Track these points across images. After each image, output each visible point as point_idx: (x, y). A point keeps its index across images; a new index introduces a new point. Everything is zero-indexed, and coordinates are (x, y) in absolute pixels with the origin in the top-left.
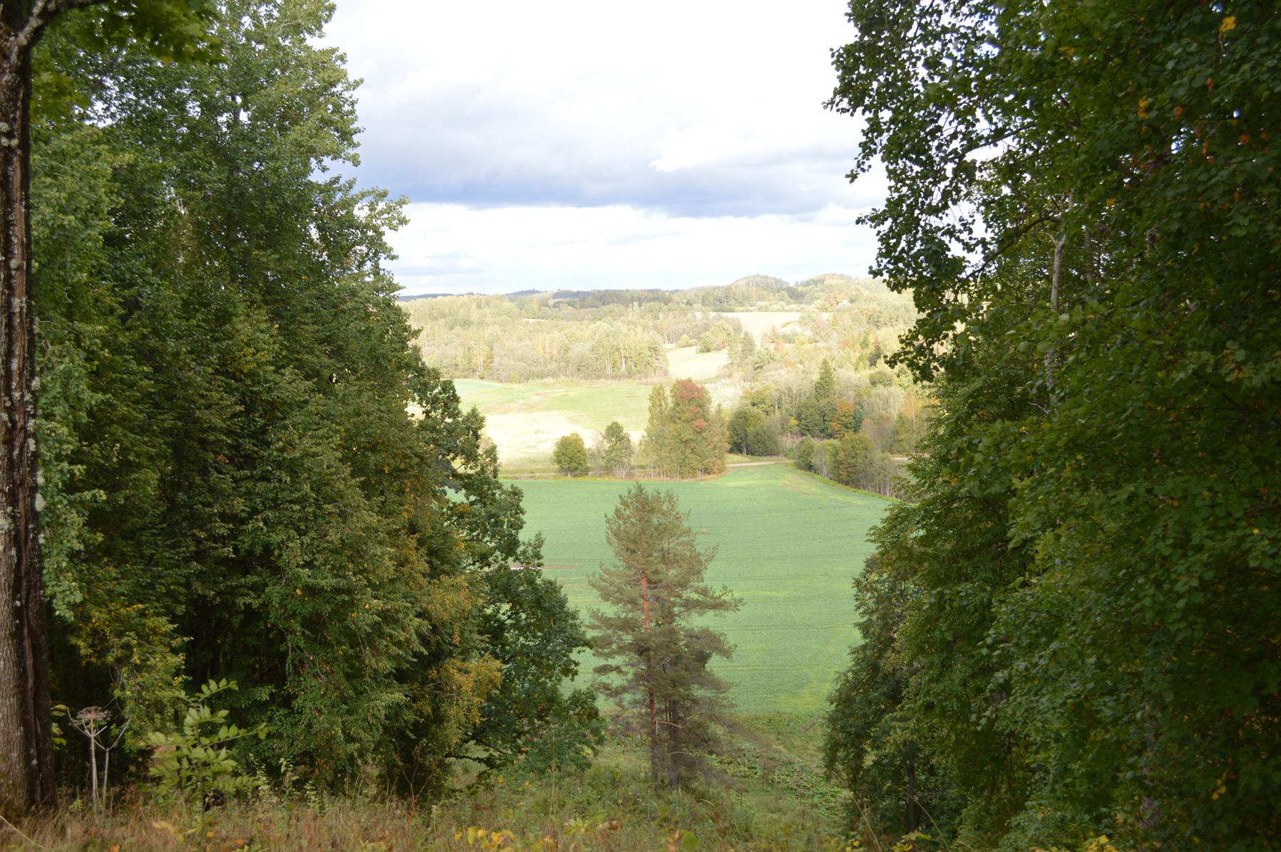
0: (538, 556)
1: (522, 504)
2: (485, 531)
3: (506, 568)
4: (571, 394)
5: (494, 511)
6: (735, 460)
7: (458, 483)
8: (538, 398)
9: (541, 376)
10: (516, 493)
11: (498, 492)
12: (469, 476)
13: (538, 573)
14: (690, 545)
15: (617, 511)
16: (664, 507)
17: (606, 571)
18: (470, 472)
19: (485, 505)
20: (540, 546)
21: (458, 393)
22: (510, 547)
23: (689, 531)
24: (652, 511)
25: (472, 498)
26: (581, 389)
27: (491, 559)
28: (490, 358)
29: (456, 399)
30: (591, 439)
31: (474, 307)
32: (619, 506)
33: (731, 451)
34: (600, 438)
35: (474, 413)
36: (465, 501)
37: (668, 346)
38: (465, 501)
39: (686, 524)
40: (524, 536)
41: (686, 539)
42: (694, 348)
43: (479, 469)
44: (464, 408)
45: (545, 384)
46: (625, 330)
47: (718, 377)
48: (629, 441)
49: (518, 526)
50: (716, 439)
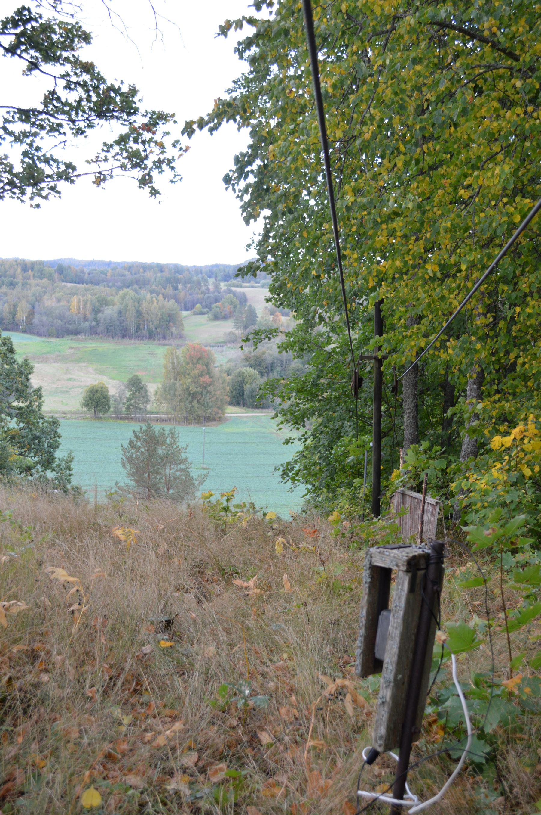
0: (69, 468)
1: (59, 431)
2: (30, 450)
3: (45, 477)
4: (100, 349)
5: (38, 434)
6: (233, 412)
7: (14, 412)
8: (72, 351)
9: (76, 333)
10: (55, 423)
11: (41, 421)
12: (20, 408)
13: (69, 481)
14: (186, 471)
15: (131, 442)
16: (168, 441)
17: (119, 488)
18: (21, 405)
19: (31, 430)
20: (71, 461)
21: (14, 347)
22: (48, 462)
23: (186, 460)
24: (157, 443)
25: (22, 425)
26: (107, 346)
27: (33, 471)
28: (32, 313)
29: (11, 351)
30: (114, 388)
31: (19, 270)
32: (133, 439)
33: (231, 403)
34: (123, 388)
35: (26, 362)
36: (16, 427)
37: (185, 313)
38: (16, 427)
39: (183, 456)
40: (59, 454)
41: (182, 466)
42: (206, 316)
43: (28, 403)
44: (19, 359)
45: (78, 340)
46: (149, 296)
47: (225, 342)
48: (146, 391)
49: (55, 446)
50: (218, 393)
